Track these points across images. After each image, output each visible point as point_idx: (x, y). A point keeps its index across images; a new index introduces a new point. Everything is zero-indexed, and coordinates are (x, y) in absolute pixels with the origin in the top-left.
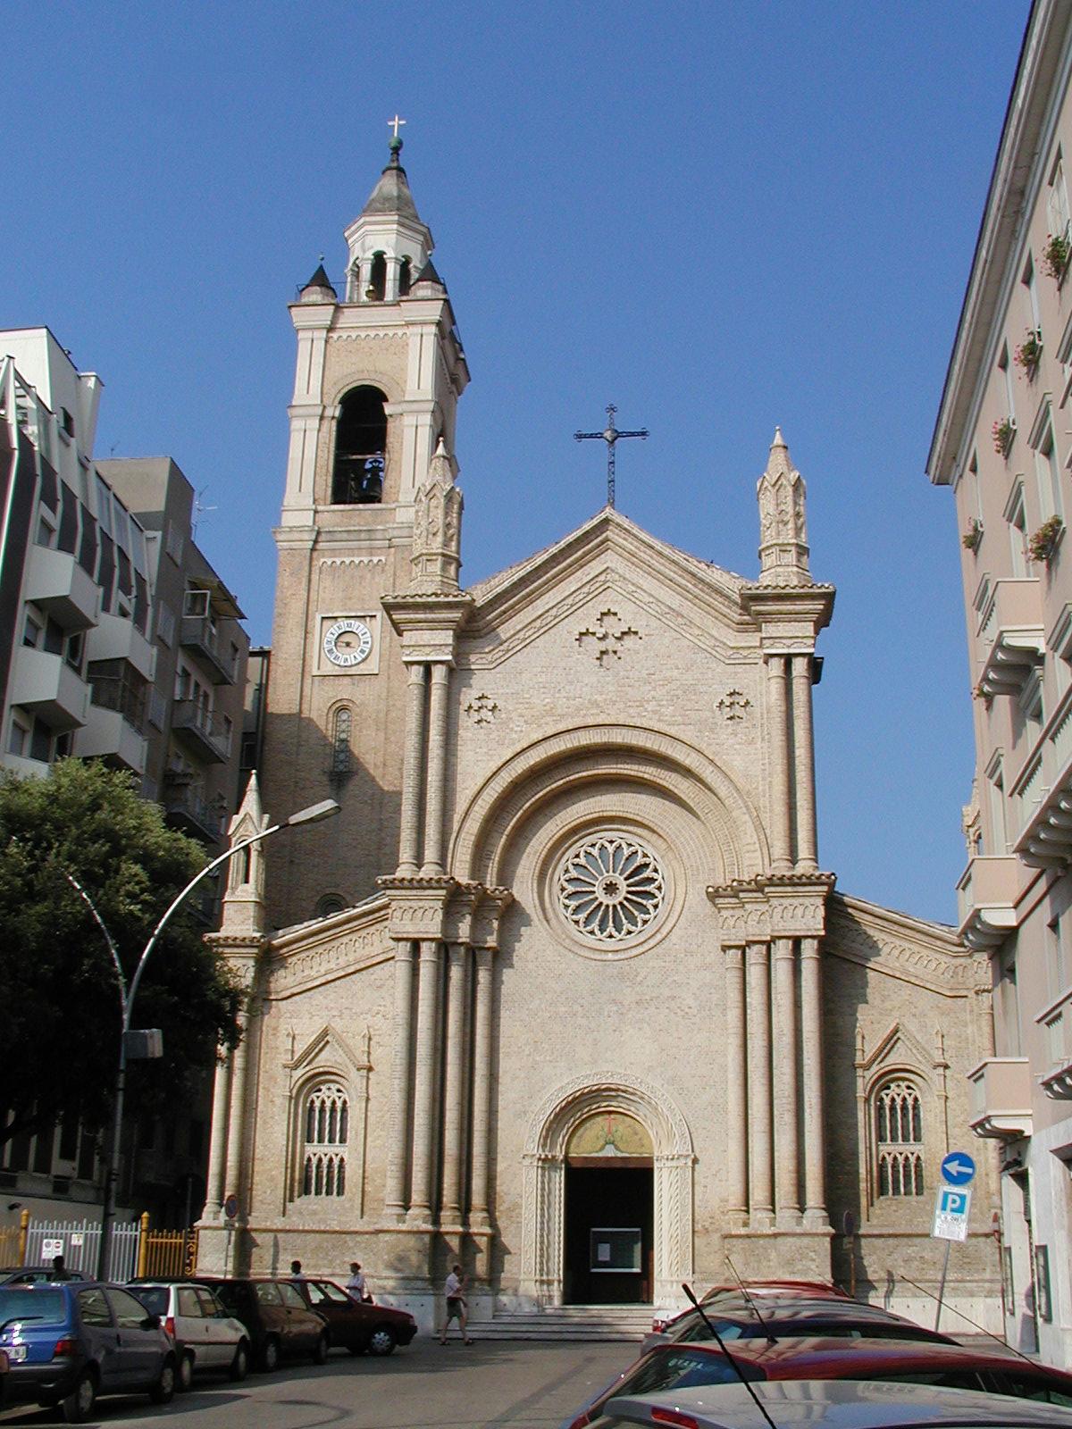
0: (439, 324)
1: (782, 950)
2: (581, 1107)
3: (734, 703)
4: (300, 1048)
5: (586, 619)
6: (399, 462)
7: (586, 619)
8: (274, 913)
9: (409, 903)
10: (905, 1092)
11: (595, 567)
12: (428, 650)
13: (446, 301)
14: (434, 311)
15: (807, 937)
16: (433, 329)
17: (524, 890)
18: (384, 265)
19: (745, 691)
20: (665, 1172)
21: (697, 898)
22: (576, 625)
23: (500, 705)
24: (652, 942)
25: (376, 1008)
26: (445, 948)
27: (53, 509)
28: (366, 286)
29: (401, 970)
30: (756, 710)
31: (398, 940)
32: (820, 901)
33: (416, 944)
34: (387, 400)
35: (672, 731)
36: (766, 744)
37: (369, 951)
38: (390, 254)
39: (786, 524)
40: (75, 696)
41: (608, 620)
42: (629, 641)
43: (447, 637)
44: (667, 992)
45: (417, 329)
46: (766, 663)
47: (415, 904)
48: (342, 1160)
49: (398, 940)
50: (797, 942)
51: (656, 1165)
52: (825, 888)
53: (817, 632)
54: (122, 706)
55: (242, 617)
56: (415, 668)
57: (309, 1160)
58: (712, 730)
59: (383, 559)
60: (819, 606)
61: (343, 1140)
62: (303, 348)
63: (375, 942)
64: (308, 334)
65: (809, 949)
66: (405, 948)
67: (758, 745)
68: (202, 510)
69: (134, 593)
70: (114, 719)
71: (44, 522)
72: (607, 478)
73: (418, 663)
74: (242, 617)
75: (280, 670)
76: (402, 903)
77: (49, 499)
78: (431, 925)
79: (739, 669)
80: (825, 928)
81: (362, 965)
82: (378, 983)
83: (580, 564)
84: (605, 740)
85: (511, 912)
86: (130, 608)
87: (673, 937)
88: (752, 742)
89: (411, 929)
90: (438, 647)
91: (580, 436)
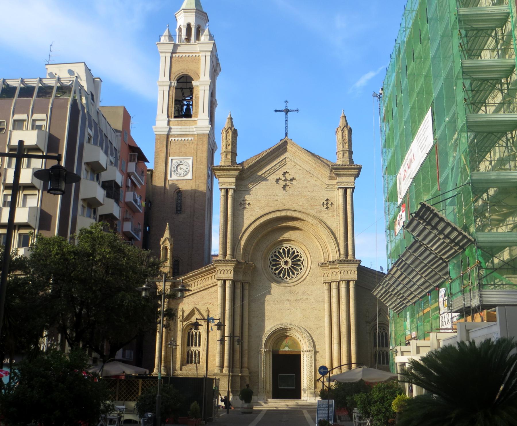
0: (211, 52)
1: (343, 285)
2: (281, 335)
3: (327, 204)
4: (186, 314)
5: (279, 175)
6: (197, 103)
7: (279, 175)
8: (178, 269)
9: (222, 268)
10: (383, 331)
11: (283, 157)
12: (227, 184)
13: (214, 43)
14: (210, 47)
15: (351, 280)
16: (209, 54)
17: (260, 265)
18: (191, 29)
19: (331, 199)
20: (305, 356)
21: (315, 266)
22: (275, 177)
23: (251, 202)
24: (300, 281)
25: (210, 302)
26: (234, 283)
27: (91, 130)
28: (184, 36)
29: (219, 289)
30: (335, 205)
31: (219, 280)
32: (356, 269)
33: (225, 282)
34: (193, 80)
35: (307, 212)
36: (338, 217)
37: (208, 283)
38: (193, 24)
39: (346, 144)
40: (100, 194)
41: (287, 175)
42: (294, 182)
43: (233, 180)
44: (305, 297)
45: (204, 54)
46: (338, 189)
47: (224, 268)
48: (199, 352)
49: (219, 280)
50: (348, 282)
51: (302, 353)
52: (357, 265)
53: (355, 180)
54: (436, 302)
55: (147, 161)
56: (223, 190)
57: (192, 352)
58: (320, 212)
59: (193, 138)
60: (356, 172)
61: (199, 345)
62: (162, 60)
63: (211, 280)
64: (164, 55)
65: (352, 285)
66: (220, 283)
67: (336, 217)
68: (133, 123)
69: (114, 156)
70: (112, 201)
71: (89, 134)
72: (284, 126)
73: (224, 189)
74: (147, 161)
75: (156, 178)
76: (220, 268)
77: (90, 127)
78: (230, 276)
79: (329, 192)
80: (357, 278)
81: (206, 287)
82: (211, 293)
83: (278, 156)
84: (285, 214)
85: (255, 270)
86: (113, 161)
87: (307, 279)
88: (333, 216)
89: (223, 276)
90: (230, 183)
91: (276, 111)
